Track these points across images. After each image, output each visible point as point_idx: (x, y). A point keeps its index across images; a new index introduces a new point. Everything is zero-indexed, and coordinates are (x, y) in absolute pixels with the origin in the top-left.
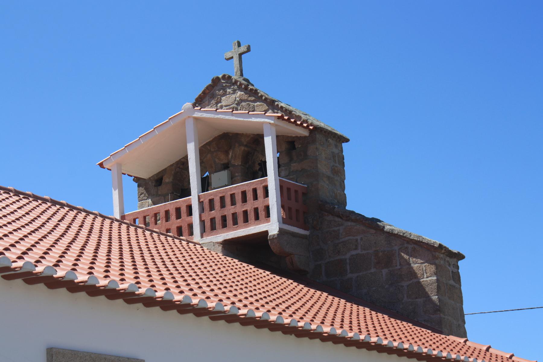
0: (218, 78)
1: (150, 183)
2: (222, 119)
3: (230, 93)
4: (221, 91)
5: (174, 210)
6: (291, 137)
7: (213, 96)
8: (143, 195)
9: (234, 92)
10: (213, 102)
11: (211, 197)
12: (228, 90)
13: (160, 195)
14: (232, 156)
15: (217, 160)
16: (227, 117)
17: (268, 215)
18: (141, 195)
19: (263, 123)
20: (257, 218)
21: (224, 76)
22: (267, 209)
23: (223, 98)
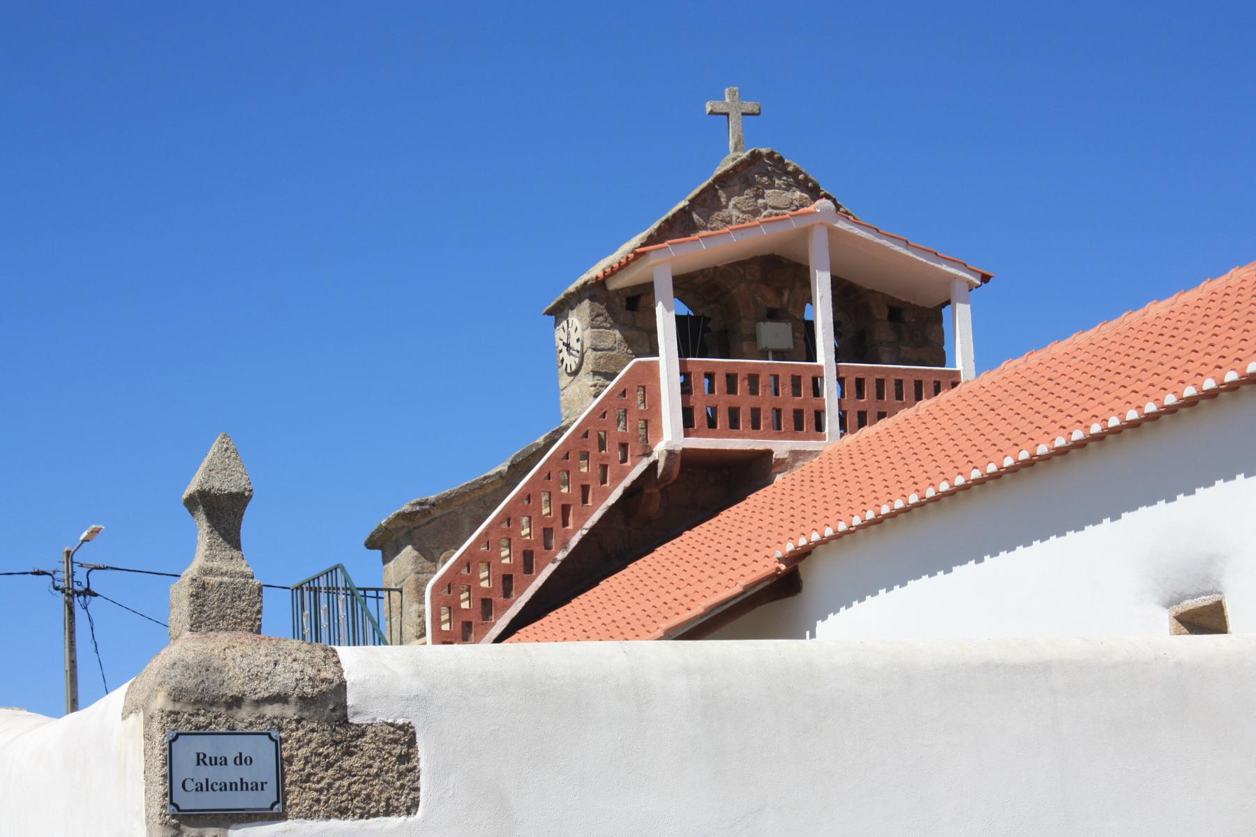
0: (760, 153)
1: (617, 300)
2: (883, 247)
3: (780, 188)
4: (766, 178)
5: (789, 379)
6: (898, 300)
7: (748, 183)
8: (601, 318)
9: (788, 187)
10: (749, 192)
11: (860, 376)
12: (777, 181)
13: (639, 329)
14: (789, 300)
15: (759, 299)
16: (897, 248)
17: (819, 427)
18: (597, 316)
19: (955, 277)
20: (799, 426)
21: (770, 155)
22: (819, 416)
23: (767, 192)
